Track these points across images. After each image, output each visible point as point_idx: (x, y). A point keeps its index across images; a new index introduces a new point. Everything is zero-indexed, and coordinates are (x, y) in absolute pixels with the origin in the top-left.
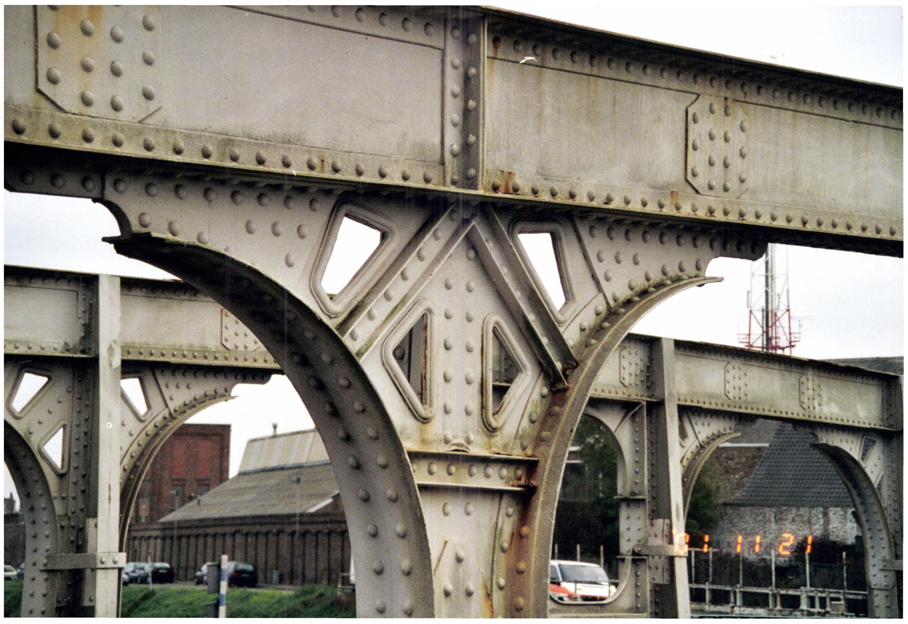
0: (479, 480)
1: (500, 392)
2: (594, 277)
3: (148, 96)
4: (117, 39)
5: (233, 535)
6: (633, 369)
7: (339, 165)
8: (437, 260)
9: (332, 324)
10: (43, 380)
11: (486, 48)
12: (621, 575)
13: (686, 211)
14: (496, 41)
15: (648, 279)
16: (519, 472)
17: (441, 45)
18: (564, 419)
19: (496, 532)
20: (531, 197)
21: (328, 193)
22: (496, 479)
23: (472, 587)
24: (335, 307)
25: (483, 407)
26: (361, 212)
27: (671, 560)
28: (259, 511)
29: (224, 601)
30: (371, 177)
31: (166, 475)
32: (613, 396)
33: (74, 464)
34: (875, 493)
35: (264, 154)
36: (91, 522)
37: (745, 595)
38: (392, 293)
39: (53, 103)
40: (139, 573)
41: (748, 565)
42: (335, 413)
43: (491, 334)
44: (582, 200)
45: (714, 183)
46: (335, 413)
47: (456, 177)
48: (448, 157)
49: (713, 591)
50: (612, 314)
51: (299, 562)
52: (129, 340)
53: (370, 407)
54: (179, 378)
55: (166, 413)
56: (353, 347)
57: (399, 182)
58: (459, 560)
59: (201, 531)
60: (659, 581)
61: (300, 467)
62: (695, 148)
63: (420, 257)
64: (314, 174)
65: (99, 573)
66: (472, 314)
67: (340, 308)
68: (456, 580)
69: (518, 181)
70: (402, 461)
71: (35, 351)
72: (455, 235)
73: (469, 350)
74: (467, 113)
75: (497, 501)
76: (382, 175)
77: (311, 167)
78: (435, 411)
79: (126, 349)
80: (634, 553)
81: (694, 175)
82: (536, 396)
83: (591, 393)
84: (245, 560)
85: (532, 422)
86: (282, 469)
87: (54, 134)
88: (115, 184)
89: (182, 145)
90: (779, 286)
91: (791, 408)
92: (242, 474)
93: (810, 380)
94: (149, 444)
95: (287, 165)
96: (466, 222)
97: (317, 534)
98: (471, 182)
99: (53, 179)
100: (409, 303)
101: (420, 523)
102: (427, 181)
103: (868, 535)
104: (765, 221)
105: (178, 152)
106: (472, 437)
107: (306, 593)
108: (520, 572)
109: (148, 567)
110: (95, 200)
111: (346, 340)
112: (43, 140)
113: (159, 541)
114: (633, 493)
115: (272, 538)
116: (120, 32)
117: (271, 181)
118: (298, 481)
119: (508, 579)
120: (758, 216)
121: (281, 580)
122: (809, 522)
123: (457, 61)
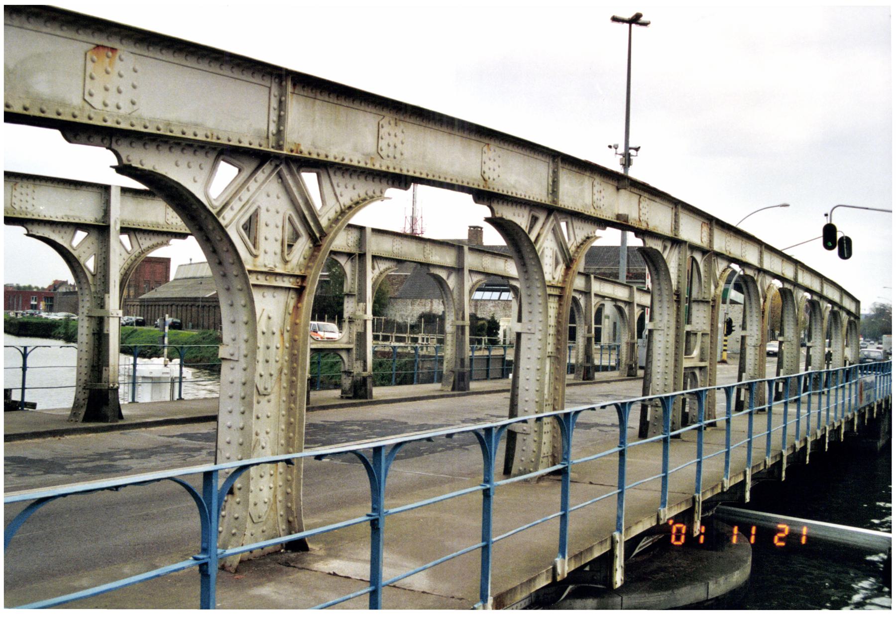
0: (279, 283)
1: (290, 246)
2: (335, 194)
3: (133, 103)
4: (121, 76)
5: (172, 305)
6: (353, 239)
7: (220, 136)
8: (264, 182)
9: (214, 212)
10: (85, 234)
11: (290, 88)
12: (344, 328)
13: (377, 167)
14: (294, 85)
15: (359, 196)
16: (298, 280)
17: (269, 85)
18: (319, 257)
19: (287, 304)
20: (308, 156)
21: (214, 149)
22: (287, 283)
23: (275, 330)
24: (216, 204)
25: (283, 251)
26: (228, 158)
27: (365, 321)
28: (183, 295)
29: (167, 335)
30: (234, 143)
31: (142, 279)
32: (343, 250)
33: (99, 271)
34: (451, 292)
35: (185, 130)
36: (107, 296)
37: (396, 337)
38: (242, 197)
39: (91, 105)
40: (130, 321)
41: (399, 325)
42: (214, 251)
43: (287, 220)
44: (331, 159)
45: (390, 155)
46: (214, 251)
47: (274, 145)
48: (270, 135)
49: (383, 336)
50: (343, 213)
51: (201, 319)
52: (124, 218)
53: (230, 249)
54: (146, 236)
55: (140, 251)
56: (223, 223)
57: (247, 145)
58: (269, 318)
59: (157, 303)
60: (360, 330)
61: (202, 277)
62: (382, 138)
63: (256, 181)
64: (209, 140)
65: (111, 319)
66: (279, 210)
67: (218, 204)
68: (268, 328)
69: (302, 148)
70: (244, 274)
71: (82, 221)
72: (273, 171)
73: (277, 227)
74: (280, 116)
75: (287, 292)
76: (240, 142)
77: (207, 137)
78: (261, 252)
79: (122, 222)
80: (349, 318)
81: (381, 150)
82: (307, 247)
83: (331, 248)
84: (177, 318)
85: (305, 259)
86: (194, 278)
87: (90, 118)
88: (116, 142)
89: (148, 124)
90: (418, 206)
91: (420, 258)
92: (175, 280)
93: (428, 247)
94: (132, 264)
95: (195, 135)
96: (277, 166)
97: (209, 306)
98: (280, 147)
99: (89, 138)
100: (251, 202)
101: (252, 301)
102: (260, 146)
103: (447, 310)
104: (411, 173)
105: (146, 127)
106: (277, 265)
107: (204, 333)
108: (296, 324)
109: (134, 318)
110: (107, 148)
111: (220, 220)
112: (85, 121)
113: (139, 307)
114: (350, 292)
115: (189, 308)
116: (122, 72)
117: (188, 143)
118: (201, 283)
119: (291, 327)
120: (408, 171)
121: (193, 327)
122: (425, 305)
123: (276, 93)
